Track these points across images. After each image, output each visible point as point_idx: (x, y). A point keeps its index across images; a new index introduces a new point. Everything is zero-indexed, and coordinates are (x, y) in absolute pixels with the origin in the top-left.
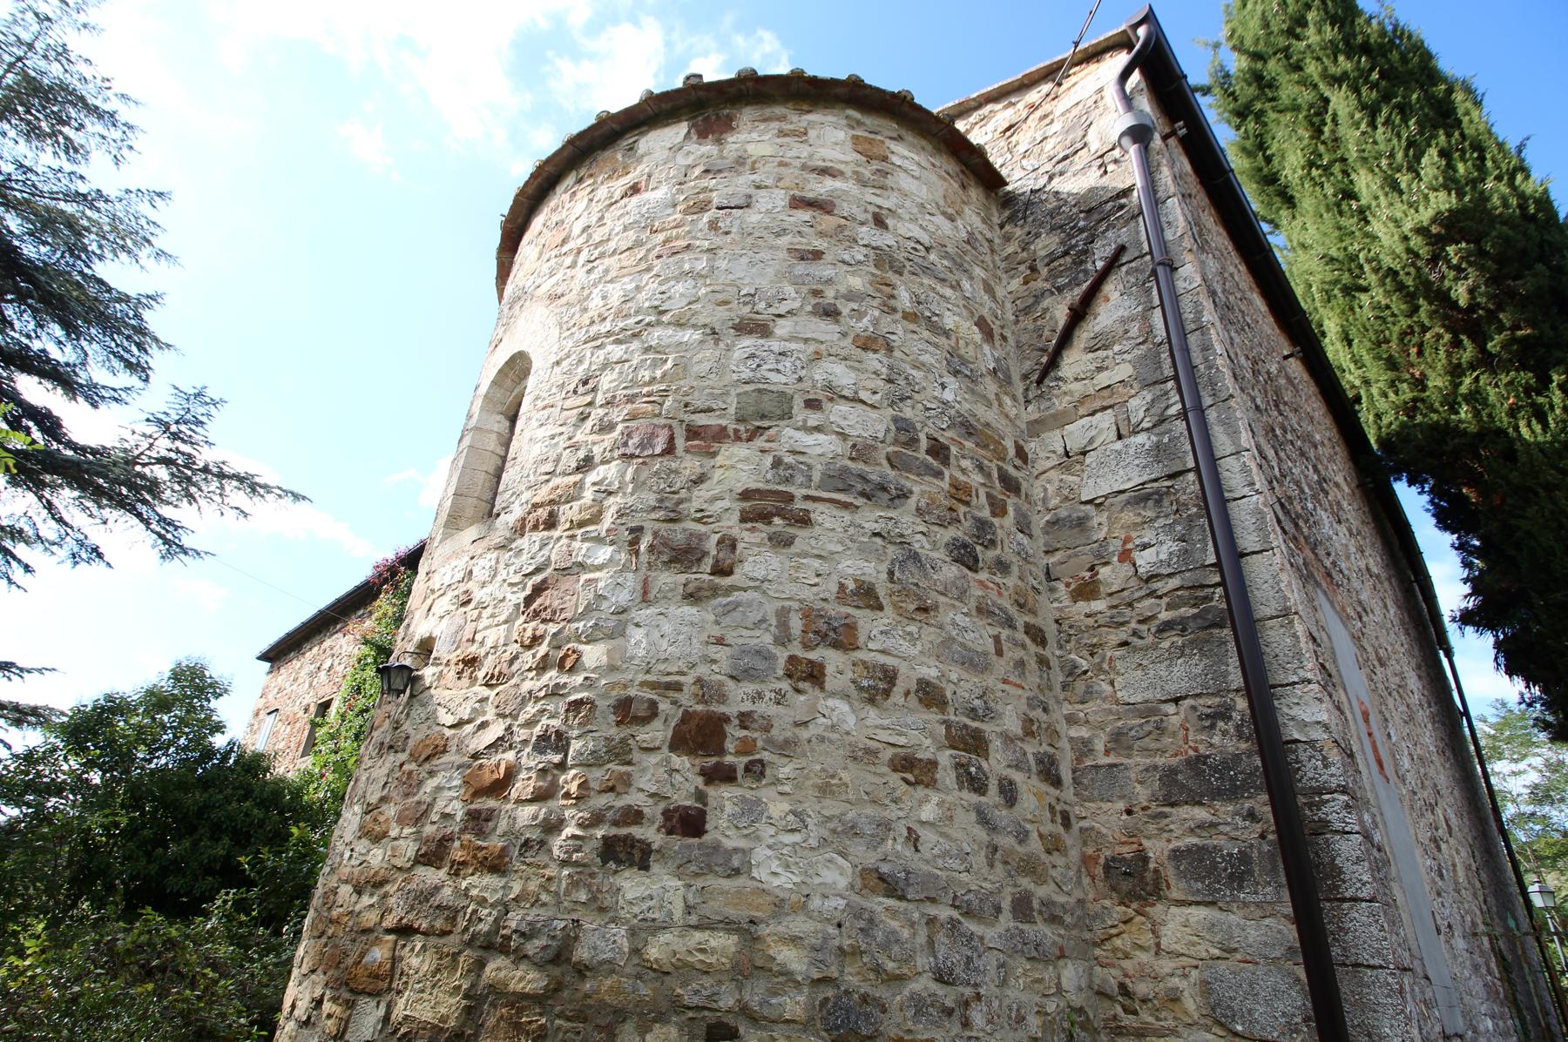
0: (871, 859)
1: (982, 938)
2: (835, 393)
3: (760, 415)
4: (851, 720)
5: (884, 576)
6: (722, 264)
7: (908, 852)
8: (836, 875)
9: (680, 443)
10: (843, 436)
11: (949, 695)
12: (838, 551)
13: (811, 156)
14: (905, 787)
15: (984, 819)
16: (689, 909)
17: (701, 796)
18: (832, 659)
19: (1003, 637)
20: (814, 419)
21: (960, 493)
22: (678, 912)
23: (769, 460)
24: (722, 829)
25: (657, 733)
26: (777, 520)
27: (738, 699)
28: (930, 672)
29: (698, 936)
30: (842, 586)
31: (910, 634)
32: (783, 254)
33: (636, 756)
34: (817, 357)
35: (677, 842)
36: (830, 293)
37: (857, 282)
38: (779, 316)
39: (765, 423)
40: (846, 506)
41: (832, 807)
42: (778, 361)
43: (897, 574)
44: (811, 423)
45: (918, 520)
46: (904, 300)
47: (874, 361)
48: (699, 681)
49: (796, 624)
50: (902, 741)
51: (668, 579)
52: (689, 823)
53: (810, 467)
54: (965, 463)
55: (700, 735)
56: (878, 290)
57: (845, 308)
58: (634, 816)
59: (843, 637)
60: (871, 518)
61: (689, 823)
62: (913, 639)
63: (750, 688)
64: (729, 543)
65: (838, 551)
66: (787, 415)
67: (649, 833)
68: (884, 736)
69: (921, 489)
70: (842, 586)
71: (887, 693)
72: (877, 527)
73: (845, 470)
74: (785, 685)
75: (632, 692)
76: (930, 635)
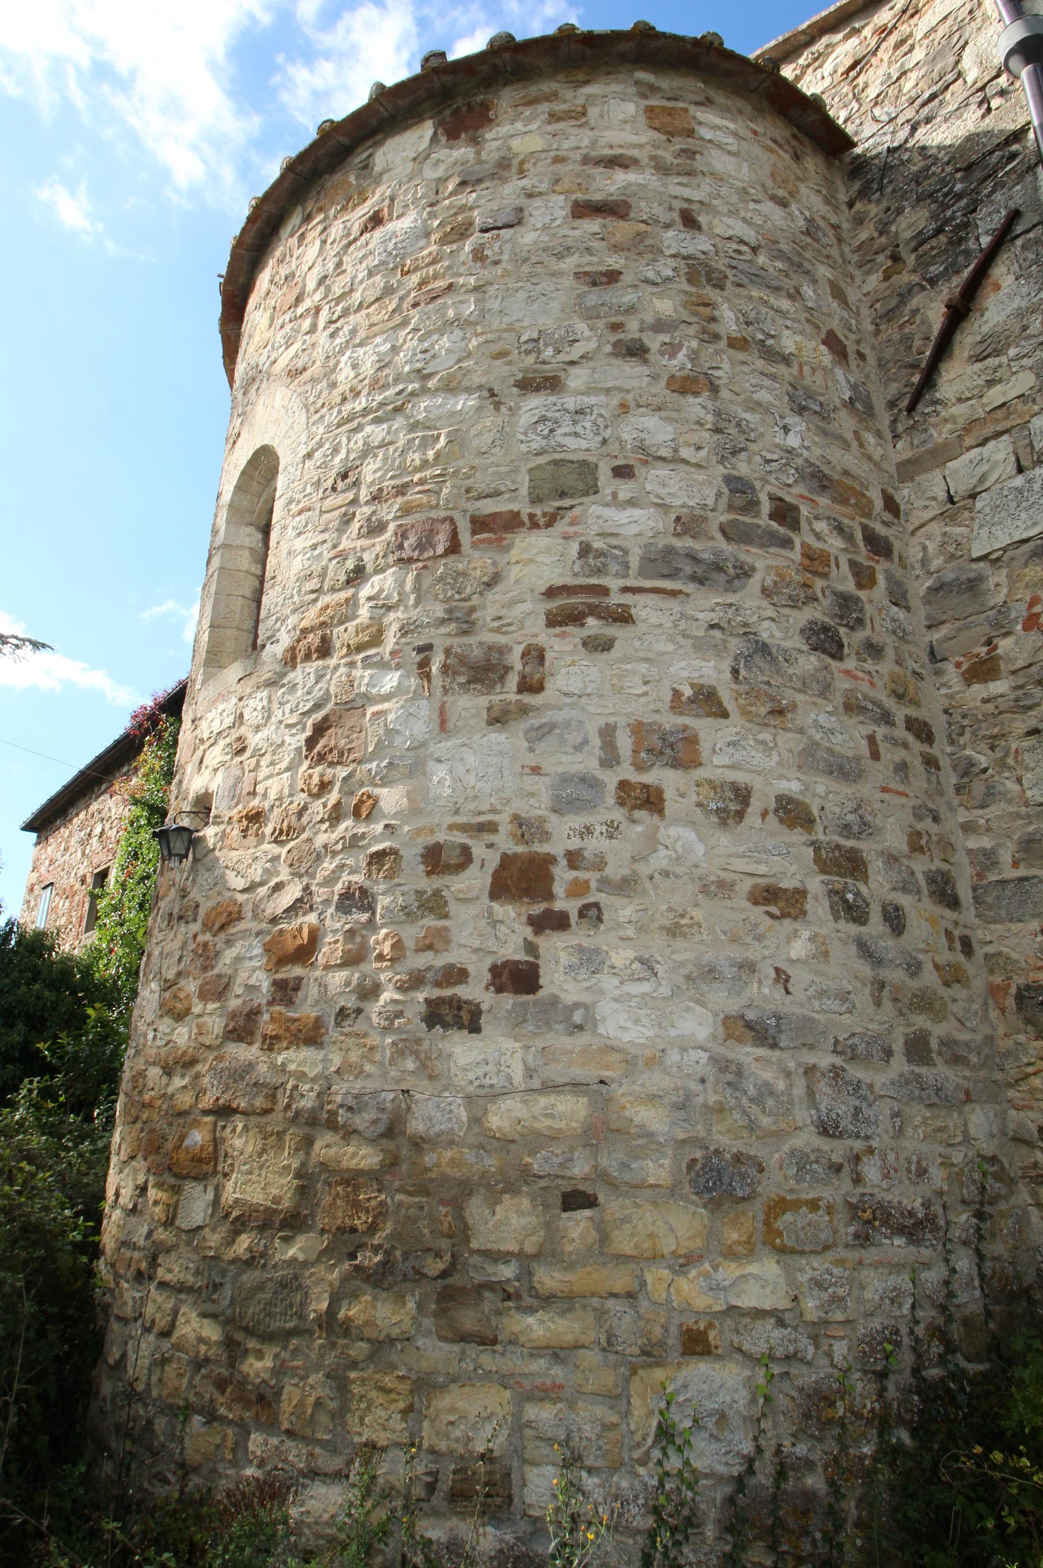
0: (734, 1006)
1: (871, 1086)
2: (650, 457)
3: (564, 485)
4: (700, 849)
5: (728, 676)
6: (495, 305)
7: (779, 993)
8: (696, 1025)
9: (465, 537)
10: (663, 507)
11: (815, 811)
12: (666, 651)
13: (594, 143)
14: (769, 921)
15: (865, 950)
16: (529, 1073)
17: (531, 948)
18: (667, 779)
19: (879, 737)
20: (625, 489)
21: (816, 562)
22: (518, 1078)
23: (574, 548)
24: (558, 980)
25: (476, 880)
26: (591, 621)
27: (562, 836)
28: (792, 787)
29: (543, 1101)
30: (677, 694)
31: (763, 742)
32: (569, 282)
33: (453, 908)
34: (624, 408)
35: (508, 1000)
36: (633, 325)
37: (665, 306)
38: (572, 363)
39: (567, 502)
40: (674, 593)
41: (685, 952)
42: (575, 422)
43: (743, 672)
44: (622, 496)
45: (765, 603)
46: (729, 322)
47: (696, 406)
48: (518, 820)
49: (624, 742)
50: (762, 869)
51: (471, 705)
52: (519, 978)
53: (626, 552)
54: (821, 526)
55: (523, 879)
56: (694, 314)
57: (654, 342)
58: (458, 975)
59: (681, 752)
60: (705, 604)
61: (519, 978)
62: (767, 748)
63: (576, 821)
64: (536, 655)
65: (666, 651)
66: (592, 489)
67: (474, 990)
68: (740, 865)
69: (765, 564)
70: (677, 694)
71: (740, 815)
72: (714, 617)
73: (669, 551)
74: (618, 815)
75: (441, 837)
76: (788, 741)
